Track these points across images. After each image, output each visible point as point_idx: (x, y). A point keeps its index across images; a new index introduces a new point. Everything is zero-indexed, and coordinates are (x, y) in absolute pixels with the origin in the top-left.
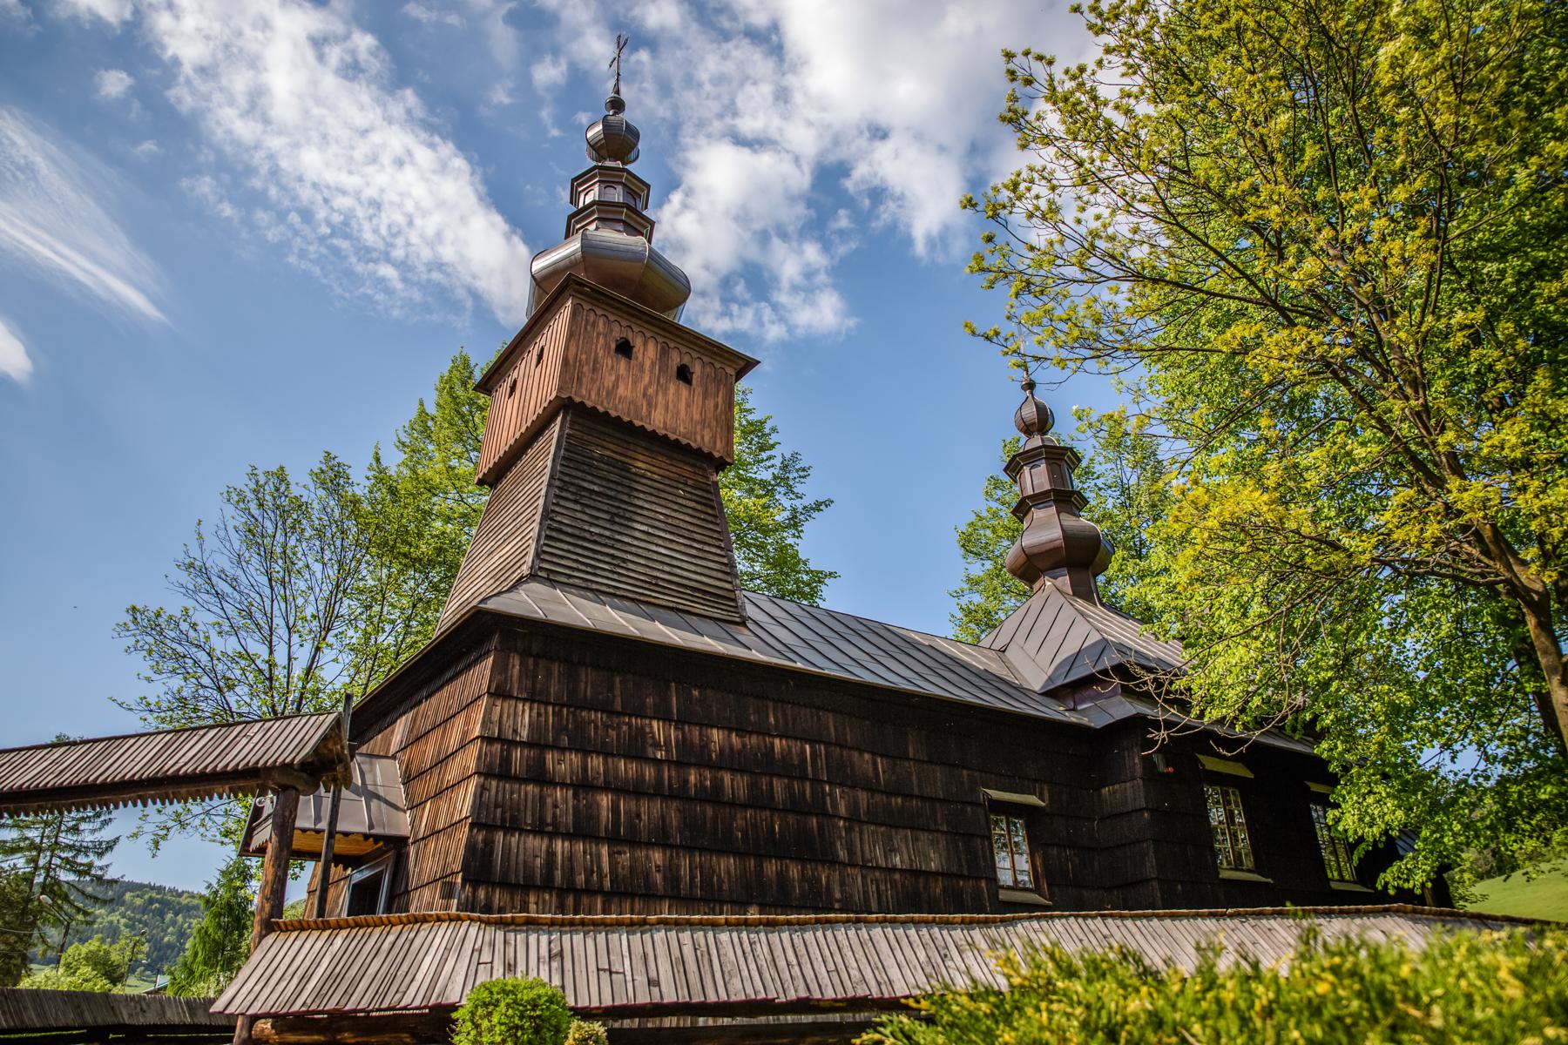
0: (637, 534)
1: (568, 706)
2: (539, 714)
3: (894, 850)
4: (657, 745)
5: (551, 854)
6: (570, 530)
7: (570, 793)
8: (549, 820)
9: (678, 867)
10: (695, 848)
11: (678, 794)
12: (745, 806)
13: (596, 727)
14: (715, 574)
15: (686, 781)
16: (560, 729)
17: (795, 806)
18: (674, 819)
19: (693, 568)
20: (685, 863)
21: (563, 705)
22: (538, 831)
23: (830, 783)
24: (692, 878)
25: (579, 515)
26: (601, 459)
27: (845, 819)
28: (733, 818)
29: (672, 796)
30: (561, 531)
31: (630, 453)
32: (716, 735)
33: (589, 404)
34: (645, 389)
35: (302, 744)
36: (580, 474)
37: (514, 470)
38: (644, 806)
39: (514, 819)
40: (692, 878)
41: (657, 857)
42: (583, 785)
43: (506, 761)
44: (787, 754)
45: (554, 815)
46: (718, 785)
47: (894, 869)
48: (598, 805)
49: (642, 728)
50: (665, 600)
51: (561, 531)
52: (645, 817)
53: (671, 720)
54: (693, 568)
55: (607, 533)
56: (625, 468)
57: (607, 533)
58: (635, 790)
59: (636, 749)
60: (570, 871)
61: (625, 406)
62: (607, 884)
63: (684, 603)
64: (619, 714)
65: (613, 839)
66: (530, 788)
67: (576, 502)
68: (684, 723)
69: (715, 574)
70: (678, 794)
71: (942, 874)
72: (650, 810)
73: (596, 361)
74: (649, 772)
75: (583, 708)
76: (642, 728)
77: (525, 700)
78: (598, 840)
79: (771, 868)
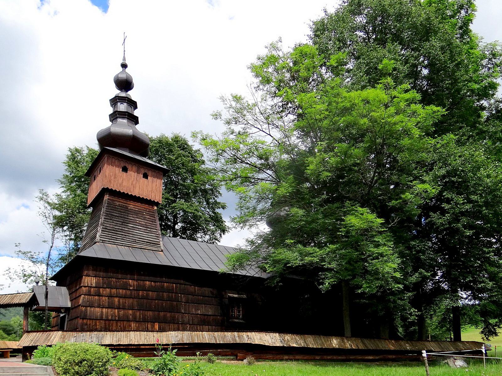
0: (129, 227)
1: (106, 278)
2: (98, 280)
3: (198, 310)
4: (131, 286)
5: (102, 312)
6: (109, 228)
7: (107, 298)
10: (141, 310)
11: (137, 297)
12: (155, 300)
13: (114, 282)
14: (154, 237)
15: (139, 294)
16: (104, 283)
17: (170, 299)
19: (147, 236)
20: (138, 314)
21: (105, 277)
22: (99, 307)
23: (180, 294)
24: (140, 317)
25: (112, 223)
26: (119, 206)
27: (184, 302)
28: (152, 302)
30: (106, 229)
31: (128, 203)
33: (114, 189)
34: (132, 182)
35: (27, 299)
36: (112, 211)
37: (97, 195)
38: (127, 300)
39: (92, 304)
40: (140, 317)
41: (130, 312)
42: (110, 296)
43: (90, 291)
46: (148, 295)
47: (198, 314)
48: (115, 301)
49: (127, 282)
50: (138, 246)
51: (106, 229)
53: (135, 280)
54: (147, 236)
55: (121, 228)
56: (127, 207)
57: (121, 228)
58: (125, 297)
59: (125, 287)
60: (107, 316)
61: (126, 188)
62: (117, 318)
63: (144, 247)
64: (120, 279)
65: (119, 308)
66: (96, 297)
67: (111, 219)
68: (138, 280)
69: (154, 237)
70: (137, 297)
71: (213, 315)
72: (129, 302)
73: (115, 175)
75: (110, 278)
76: (127, 282)
77: (94, 277)
78: (115, 308)
79: (162, 314)
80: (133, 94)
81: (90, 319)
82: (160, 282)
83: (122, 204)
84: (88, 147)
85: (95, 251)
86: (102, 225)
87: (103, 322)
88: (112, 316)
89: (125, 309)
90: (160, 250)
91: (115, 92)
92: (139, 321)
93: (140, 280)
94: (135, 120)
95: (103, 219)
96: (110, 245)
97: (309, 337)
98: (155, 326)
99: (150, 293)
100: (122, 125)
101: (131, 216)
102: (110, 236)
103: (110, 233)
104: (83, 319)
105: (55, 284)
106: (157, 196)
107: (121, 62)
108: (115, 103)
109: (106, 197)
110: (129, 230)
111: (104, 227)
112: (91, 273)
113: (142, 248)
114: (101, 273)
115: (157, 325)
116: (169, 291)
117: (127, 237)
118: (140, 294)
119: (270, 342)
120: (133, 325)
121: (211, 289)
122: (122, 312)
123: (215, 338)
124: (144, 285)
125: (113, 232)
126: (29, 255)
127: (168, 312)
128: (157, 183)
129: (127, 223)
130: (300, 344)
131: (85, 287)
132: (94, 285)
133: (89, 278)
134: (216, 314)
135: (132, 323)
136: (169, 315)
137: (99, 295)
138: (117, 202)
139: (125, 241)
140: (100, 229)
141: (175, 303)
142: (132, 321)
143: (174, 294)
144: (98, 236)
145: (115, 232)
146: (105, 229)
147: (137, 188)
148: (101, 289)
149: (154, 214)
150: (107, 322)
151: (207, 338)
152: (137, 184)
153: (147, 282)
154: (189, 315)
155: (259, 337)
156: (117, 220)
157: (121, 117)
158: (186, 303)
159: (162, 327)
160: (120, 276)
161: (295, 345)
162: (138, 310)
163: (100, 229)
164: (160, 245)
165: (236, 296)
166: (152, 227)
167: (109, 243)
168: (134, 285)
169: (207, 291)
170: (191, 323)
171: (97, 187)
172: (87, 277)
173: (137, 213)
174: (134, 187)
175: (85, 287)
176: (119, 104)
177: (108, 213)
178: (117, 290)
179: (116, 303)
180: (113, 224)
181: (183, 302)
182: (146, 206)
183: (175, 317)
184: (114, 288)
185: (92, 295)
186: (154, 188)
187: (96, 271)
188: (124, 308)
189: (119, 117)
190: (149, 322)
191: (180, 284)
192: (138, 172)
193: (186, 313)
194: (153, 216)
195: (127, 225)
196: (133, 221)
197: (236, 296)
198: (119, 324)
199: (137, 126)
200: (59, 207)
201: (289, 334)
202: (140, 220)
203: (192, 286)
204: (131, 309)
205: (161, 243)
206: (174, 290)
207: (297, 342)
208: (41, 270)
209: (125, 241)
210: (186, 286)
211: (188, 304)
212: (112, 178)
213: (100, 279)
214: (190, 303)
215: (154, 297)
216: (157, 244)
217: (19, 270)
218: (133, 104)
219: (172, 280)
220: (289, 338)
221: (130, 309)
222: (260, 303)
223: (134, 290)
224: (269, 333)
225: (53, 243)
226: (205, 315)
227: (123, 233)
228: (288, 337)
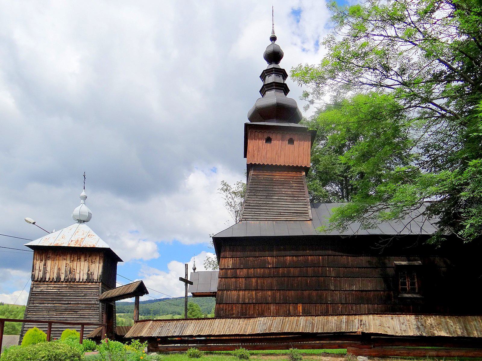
0: (274, 200)
4: (269, 263)
7: (244, 279)
8: (238, 287)
9: (276, 295)
10: (281, 290)
15: (278, 272)
18: (275, 283)
20: (278, 294)
21: (241, 257)
24: (280, 298)
27: (334, 277)
28: (293, 280)
30: (249, 205)
31: (274, 174)
41: (269, 293)
42: (247, 277)
43: (226, 273)
44: (312, 260)
45: (240, 285)
47: (353, 290)
48: (252, 282)
50: (283, 218)
51: (249, 205)
52: (266, 283)
55: (265, 202)
57: (265, 202)
60: (244, 299)
61: (270, 160)
63: (289, 218)
64: (258, 257)
65: (256, 290)
68: (278, 256)
74: (267, 271)
75: (247, 257)
77: (231, 258)
79: (306, 293)
80: (282, 65)
81: (226, 304)
82: (303, 256)
83: (268, 177)
87: (240, 306)
88: (249, 299)
89: (263, 290)
90: (308, 219)
91: (265, 66)
92: (279, 303)
93: (280, 256)
94: (286, 90)
96: (253, 222)
97: (476, 320)
98: (299, 308)
99: (292, 269)
101: (276, 187)
102: (253, 212)
103: (253, 210)
106: (304, 160)
107: (270, 35)
108: (264, 78)
110: (274, 203)
111: (248, 204)
113: (288, 219)
114: (239, 253)
115: (301, 307)
116: (314, 265)
117: (271, 211)
118: (280, 272)
119: (398, 329)
120: (272, 307)
121: (369, 258)
122: (260, 294)
123: (313, 324)
124: (285, 262)
125: (257, 208)
127: (313, 290)
128: (305, 146)
129: (272, 196)
130: (455, 332)
133: (226, 260)
134: (378, 289)
135: (272, 305)
136: (314, 293)
139: (269, 215)
141: (322, 278)
142: (271, 303)
143: (320, 269)
145: (259, 208)
148: (238, 271)
149: (302, 180)
150: (244, 306)
151: (302, 325)
152: (282, 153)
153: (288, 257)
154: (341, 292)
155: (378, 322)
156: (262, 194)
157: (268, 90)
158: (336, 277)
159: (306, 309)
160: (257, 254)
161: (443, 334)
162: (278, 290)
164: (308, 213)
165: (404, 263)
166: (300, 196)
167: (252, 220)
168: (273, 262)
169: (363, 260)
170: (343, 302)
172: (224, 259)
173: (283, 184)
174: (278, 156)
177: (252, 189)
178: (255, 269)
179: (253, 284)
180: (257, 199)
181: (332, 277)
182: (293, 174)
184: (252, 268)
185: (229, 278)
187: (233, 251)
189: (268, 90)
190: (291, 303)
192: (283, 140)
193: (337, 291)
194: (301, 183)
195: (272, 197)
196: (278, 192)
198: (257, 308)
199: (289, 96)
201: (436, 315)
202: (286, 190)
203: (343, 256)
204: (270, 290)
205: (310, 211)
206: (321, 264)
207: (448, 329)
209: (269, 215)
210: (335, 257)
211: (338, 279)
213: (237, 259)
214: (342, 277)
215: (297, 273)
218: (283, 74)
219: (318, 252)
220: (433, 322)
221: (268, 290)
223: (273, 268)
224: (397, 314)
226: (362, 291)
227: (266, 207)
228: (431, 320)
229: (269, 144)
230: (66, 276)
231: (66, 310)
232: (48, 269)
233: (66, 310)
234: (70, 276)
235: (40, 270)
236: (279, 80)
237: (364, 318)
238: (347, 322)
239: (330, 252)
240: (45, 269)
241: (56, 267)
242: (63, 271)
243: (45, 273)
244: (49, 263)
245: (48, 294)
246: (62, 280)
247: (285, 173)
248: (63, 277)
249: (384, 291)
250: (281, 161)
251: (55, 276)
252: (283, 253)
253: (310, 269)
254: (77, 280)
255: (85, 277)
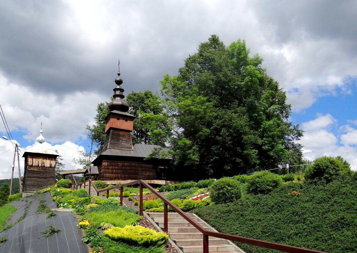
5: (109, 175)
16: (110, 164)
20: (122, 176)
26: (116, 133)
27: (141, 171)
29: (121, 170)
32: (126, 164)
41: (120, 175)
42: (112, 169)
43: (105, 168)
50: (123, 149)
58: (118, 169)
60: (111, 177)
63: (125, 149)
65: (115, 174)
74: (119, 167)
79: (132, 175)
80: (122, 86)
84: (106, 103)
85: (106, 153)
86: (110, 142)
95: (110, 140)
100: (118, 100)
104: (103, 178)
105: (93, 165)
109: (111, 131)
112: (105, 161)
116: (134, 166)
122: (116, 175)
126: (82, 152)
131: (103, 166)
132: (106, 165)
133: (105, 163)
134: (154, 175)
136: (134, 176)
137: (108, 169)
138: (115, 134)
140: (109, 144)
144: (108, 146)
146: (111, 144)
147: (123, 126)
160: (116, 161)
163: (109, 144)
165: (163, 168)
169: (150, 166)
171: (108, 125)
173: (123, 136)
175: (103, 166)
176: (117, 91)
183: (136, 177)
186: (130, 125)
188: (117, 174)
191: (139, 164)
197: (163, 168)
200: (93, 131)
205: (132, 147)
208: (87, 158)
212: (114, 123)
216: (131, 148)
217: (78, 159)
219: (136, 162)
222: (174, 170)
225: (92, 147)
226: (149, 176)
229: (118, 121)
230: (41, 165)
231: (42, 178)
232: (34, 161)
233: (42, 178)
234: (43, 165)
235: (31, 162)
236: (121, 94)
237: (154, 180)
238: (150, 181)
239: (140, 163)
240: (33, 161)
241: (37, 161)
242: (40, 163)
243: (33, 163)
244: (34, 159)
245: (34, 171)
246: (40, 166)
247: (124, 132)
248: (40, 165)
249: (156, 176)
250: (123, 128)
251: (37, 164)
252: (124, 162)
253: (133, 168)
254: (46, 167)
255: (49, 166)
